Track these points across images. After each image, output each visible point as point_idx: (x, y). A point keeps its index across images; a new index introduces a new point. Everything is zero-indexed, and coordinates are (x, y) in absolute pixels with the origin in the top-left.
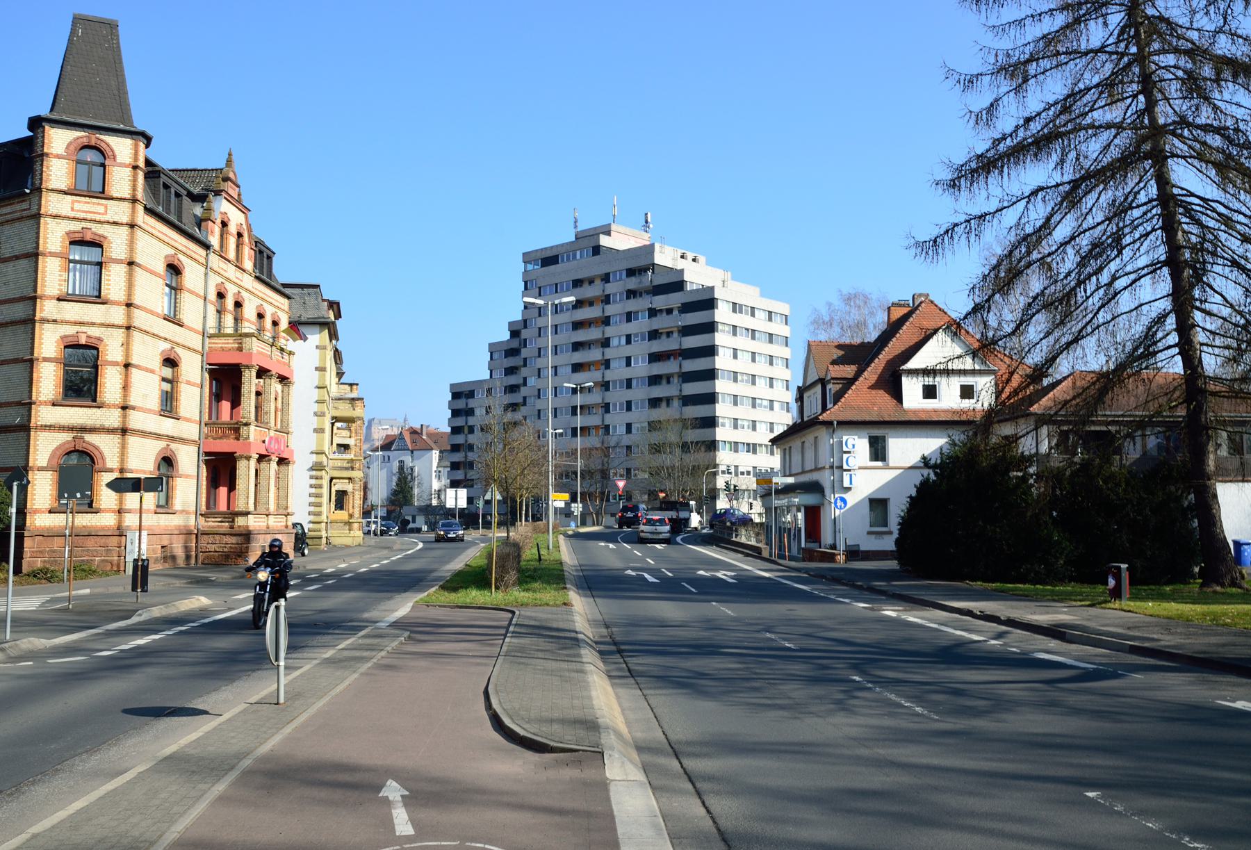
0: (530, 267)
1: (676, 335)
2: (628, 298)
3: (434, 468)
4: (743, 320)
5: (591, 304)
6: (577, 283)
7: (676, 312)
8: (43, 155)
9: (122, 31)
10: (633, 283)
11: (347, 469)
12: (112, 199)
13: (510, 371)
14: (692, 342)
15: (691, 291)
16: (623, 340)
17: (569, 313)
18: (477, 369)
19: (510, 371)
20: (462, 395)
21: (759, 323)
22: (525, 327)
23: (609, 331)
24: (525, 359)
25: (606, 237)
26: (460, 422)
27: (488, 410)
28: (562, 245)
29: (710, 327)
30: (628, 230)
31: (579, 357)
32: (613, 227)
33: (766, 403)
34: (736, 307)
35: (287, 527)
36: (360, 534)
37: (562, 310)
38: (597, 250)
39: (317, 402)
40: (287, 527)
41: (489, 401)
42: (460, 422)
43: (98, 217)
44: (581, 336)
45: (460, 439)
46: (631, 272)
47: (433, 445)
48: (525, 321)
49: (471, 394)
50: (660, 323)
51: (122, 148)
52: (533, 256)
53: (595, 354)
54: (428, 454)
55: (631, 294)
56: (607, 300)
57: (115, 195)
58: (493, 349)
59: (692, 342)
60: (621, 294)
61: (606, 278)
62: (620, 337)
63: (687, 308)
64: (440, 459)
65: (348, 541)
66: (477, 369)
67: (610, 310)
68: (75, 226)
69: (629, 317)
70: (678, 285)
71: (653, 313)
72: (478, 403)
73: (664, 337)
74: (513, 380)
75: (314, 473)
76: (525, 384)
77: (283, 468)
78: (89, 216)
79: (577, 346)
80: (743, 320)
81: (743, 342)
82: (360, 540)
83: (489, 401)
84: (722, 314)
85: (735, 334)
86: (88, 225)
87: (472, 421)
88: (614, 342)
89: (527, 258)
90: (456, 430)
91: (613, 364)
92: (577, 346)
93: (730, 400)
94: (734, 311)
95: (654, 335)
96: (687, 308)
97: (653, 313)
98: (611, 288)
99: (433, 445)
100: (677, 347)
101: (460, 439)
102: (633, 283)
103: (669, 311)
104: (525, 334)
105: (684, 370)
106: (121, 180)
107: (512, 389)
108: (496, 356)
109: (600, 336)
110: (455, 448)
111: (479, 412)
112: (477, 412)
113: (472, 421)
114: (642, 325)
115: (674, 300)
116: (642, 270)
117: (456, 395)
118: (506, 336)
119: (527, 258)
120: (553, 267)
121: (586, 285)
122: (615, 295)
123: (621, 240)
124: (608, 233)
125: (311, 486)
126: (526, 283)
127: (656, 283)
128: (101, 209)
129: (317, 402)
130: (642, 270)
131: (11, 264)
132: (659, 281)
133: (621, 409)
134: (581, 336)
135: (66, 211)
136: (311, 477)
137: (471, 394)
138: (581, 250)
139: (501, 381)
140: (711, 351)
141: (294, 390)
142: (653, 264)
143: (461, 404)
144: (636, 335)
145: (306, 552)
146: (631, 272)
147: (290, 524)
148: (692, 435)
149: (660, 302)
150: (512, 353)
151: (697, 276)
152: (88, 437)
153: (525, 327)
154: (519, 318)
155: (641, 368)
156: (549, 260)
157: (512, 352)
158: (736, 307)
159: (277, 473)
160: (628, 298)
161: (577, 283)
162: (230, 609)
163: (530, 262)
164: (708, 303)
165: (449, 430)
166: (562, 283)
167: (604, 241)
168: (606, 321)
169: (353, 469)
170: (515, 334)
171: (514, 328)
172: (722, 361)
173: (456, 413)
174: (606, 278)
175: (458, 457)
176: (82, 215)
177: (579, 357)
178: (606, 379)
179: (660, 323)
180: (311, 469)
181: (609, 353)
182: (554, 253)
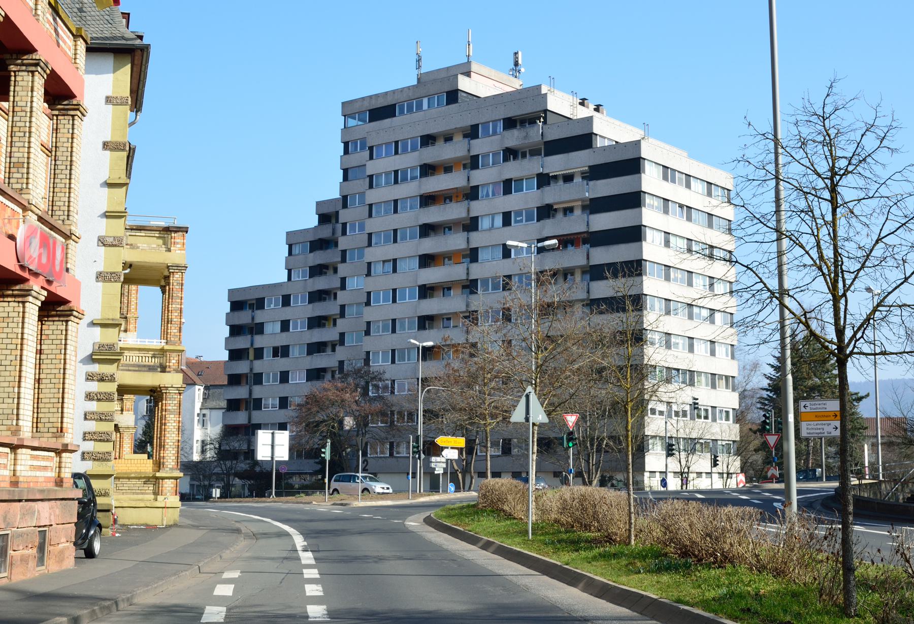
0: (352, 122)
1: (578, 212)
2: (506, 159)
3: (197, 411)
4: (675, 192)
5: (448, 169)
6: (428, 140)
7: (578, 179)
10: (514, 138)
11: (151, 369)
13: (317, 271)
14: (604, 221)
15: (604, 148)
16: (499, 221)
17: (415, 183)
18: (269, 268)
19: (317, 271)
20: (245, 306)
21: (695, 197)
22: (345, 206)
23: (477, 208)
24: (344, 252)
25: (466, 78)
26: (242, 342)
27: (285, 326)
28: (402, 90)
29: (634, 200)
30: (492, 73)
31: (430, 245)
32: (474, 67)
33: (705, 313)
34: (668, 173)
35: (59, 482)
36: (175, 500)
37: (405, 179)
38: (453, 96)
39: (107, 215)
40: (59, 482)
41: (287, 313)
42: (242, 342)
44: (434, 214)
45: (242, 367)
46: (510, 123)
47: (196, 379)
48: (345, 198)
49: (260, 304)
50: (554, 194)
52: (357, 107)
53: (456, 241)
55: (510, 154)
56: (473, 163)
58: (293, 240)
59: (604, 221)
60: (495, 154)
61: (472, 133)
62: (493, 216)
63: (596, 172)
64: (205, 398)
65: (153, 517)
66: (269, 268)
67: (479, 177)
69: (508, 186)
70: (584, 140)
71: (544, 180)
72: (271, 316)
73: (560, 215)
74: (321, 283)
75: (96, 368)
76: (343, 287)
77: (54, 327)
79: (427, 230)
80: (675, 192)
81: (676, 224)
82: (172, 516)
83: (287, 313)
84: (650, 181)
85: (666, 211)
87: (259, 341)
88: (484, 224)
89: (349, 110)
90: (236, 355)
91: (482, 255)
92: (427, 230)
93: (659, 306)
94: (665, 178)
95: (545, 212)
96: (596, 172)
97: (544, 180)
98: (479, 146)
99: (196, 379)
100: (583, 229)
101: (242, 367)
102: (514, 138)
103: (568, 178)
104: (344, 216)
105: (593, 262)
107: (317, 296)
108: (296, 250)
109: (463, 214)
110: (235, 380)
111: (273, 328)
112: (268, 329)
113: (259, 341)
114: (528, 198)
115: (578, 161)
116: (530, 120)
117: (237, 306)
118: (313, 221)
119: (349, 110)
120: (387, 122)
121: (440, 143)
122: (486, 156)
123: (481, 84)
124: (468, 74)
125: (89, 397)
126: (346, 145)
127: (550, 137)
129: (107, 215)
130: (530, 120)
132: (554, 134)
133: (275, 380)
134: (434, 214)
136: (90, 377)
137: (260, 304)
138: (430, 97)
139: (307, 284)
140: (635, 234)
142: (546, 111)
143: (244, 317)
144: (519, 213)
145: (97, 546)
146: (510, 123)
147: (67, 474)
148: (612, 358)
149: (555, 164)
150: (323, 244)
151: (611, 131)
153: (345, 206)
154: (335, 194)
156: (381, 111)
157: (319, 244)
158: (668, 173)
159: (133, 218)
160: (506, 159)
161: (428, 140)
163: (352, 116)
164: (629, 164)
165: (225, 356)
166: (405, 141)
167: (464, 84)
168: (472, 193)
169: (163, 369)
170: (325, 218)
171: (325, 211)
172: (651, 249)
173: (236, 330)
174: (472, 133)
175: (240, 392)
177: (430, 245)
178: (472, 277)
179: (554, 194)
180: (91, 359)
181: (477, 240)
182: (389, 101)
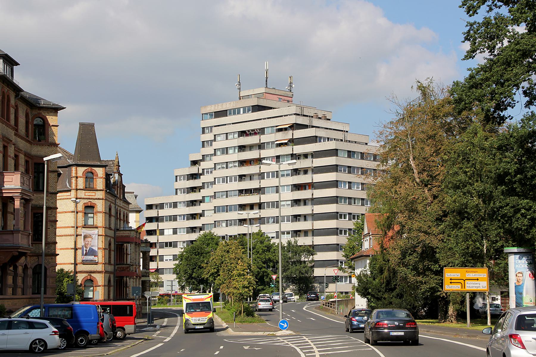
8: (105, 286)
9: (97, 128)
12: (97, 190)
43: (93, 197)
51: (100, 172)
54: (79, 311)
57: (98, 188)
68: (86, 201)
78: (90, 197)
86: (90, 200)
106: (100, 183)
128: (94, 194)
131: (63, 214)
135: (83, 196)
141: (225, 170)
152: (93, 275)
155: (289, 195)
162: (46, 244)
170: (480, 7)
176: (88, 197)
